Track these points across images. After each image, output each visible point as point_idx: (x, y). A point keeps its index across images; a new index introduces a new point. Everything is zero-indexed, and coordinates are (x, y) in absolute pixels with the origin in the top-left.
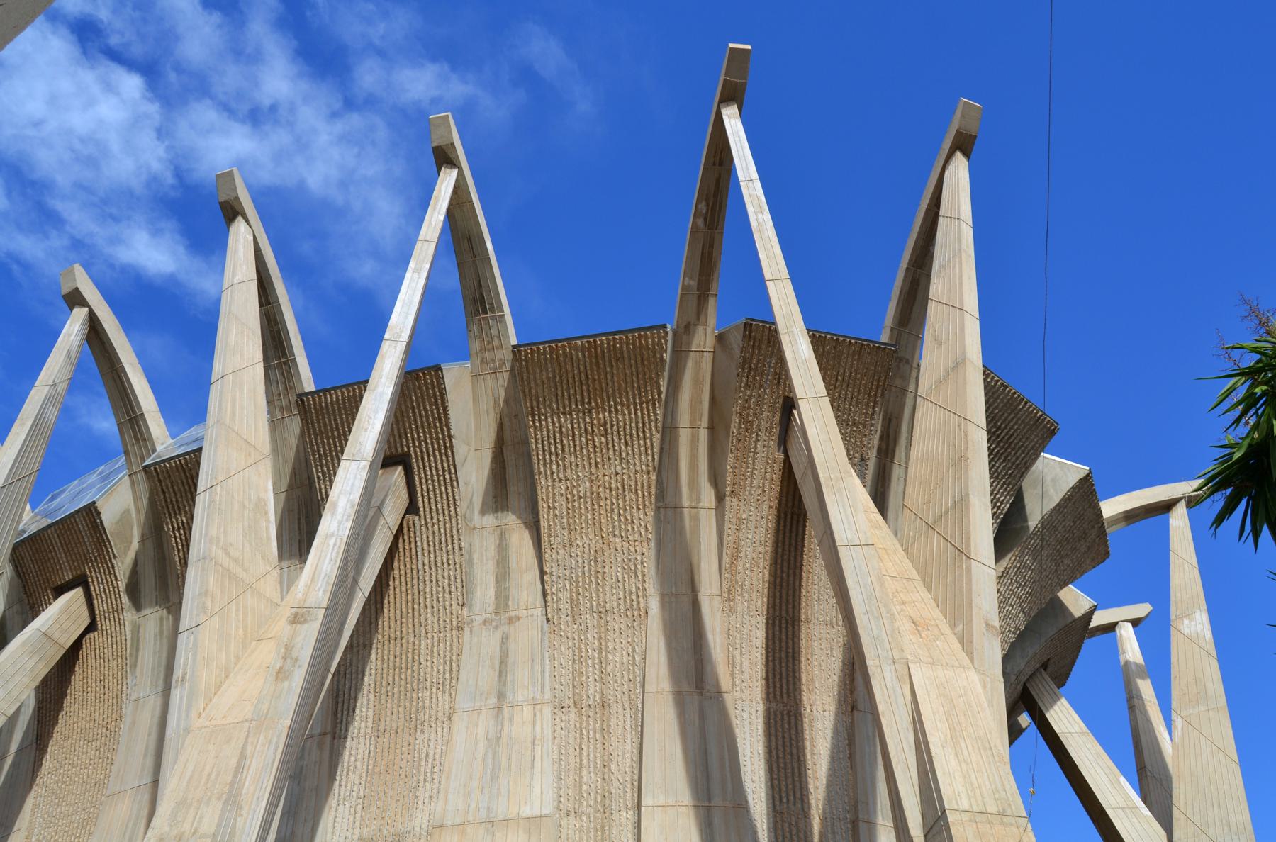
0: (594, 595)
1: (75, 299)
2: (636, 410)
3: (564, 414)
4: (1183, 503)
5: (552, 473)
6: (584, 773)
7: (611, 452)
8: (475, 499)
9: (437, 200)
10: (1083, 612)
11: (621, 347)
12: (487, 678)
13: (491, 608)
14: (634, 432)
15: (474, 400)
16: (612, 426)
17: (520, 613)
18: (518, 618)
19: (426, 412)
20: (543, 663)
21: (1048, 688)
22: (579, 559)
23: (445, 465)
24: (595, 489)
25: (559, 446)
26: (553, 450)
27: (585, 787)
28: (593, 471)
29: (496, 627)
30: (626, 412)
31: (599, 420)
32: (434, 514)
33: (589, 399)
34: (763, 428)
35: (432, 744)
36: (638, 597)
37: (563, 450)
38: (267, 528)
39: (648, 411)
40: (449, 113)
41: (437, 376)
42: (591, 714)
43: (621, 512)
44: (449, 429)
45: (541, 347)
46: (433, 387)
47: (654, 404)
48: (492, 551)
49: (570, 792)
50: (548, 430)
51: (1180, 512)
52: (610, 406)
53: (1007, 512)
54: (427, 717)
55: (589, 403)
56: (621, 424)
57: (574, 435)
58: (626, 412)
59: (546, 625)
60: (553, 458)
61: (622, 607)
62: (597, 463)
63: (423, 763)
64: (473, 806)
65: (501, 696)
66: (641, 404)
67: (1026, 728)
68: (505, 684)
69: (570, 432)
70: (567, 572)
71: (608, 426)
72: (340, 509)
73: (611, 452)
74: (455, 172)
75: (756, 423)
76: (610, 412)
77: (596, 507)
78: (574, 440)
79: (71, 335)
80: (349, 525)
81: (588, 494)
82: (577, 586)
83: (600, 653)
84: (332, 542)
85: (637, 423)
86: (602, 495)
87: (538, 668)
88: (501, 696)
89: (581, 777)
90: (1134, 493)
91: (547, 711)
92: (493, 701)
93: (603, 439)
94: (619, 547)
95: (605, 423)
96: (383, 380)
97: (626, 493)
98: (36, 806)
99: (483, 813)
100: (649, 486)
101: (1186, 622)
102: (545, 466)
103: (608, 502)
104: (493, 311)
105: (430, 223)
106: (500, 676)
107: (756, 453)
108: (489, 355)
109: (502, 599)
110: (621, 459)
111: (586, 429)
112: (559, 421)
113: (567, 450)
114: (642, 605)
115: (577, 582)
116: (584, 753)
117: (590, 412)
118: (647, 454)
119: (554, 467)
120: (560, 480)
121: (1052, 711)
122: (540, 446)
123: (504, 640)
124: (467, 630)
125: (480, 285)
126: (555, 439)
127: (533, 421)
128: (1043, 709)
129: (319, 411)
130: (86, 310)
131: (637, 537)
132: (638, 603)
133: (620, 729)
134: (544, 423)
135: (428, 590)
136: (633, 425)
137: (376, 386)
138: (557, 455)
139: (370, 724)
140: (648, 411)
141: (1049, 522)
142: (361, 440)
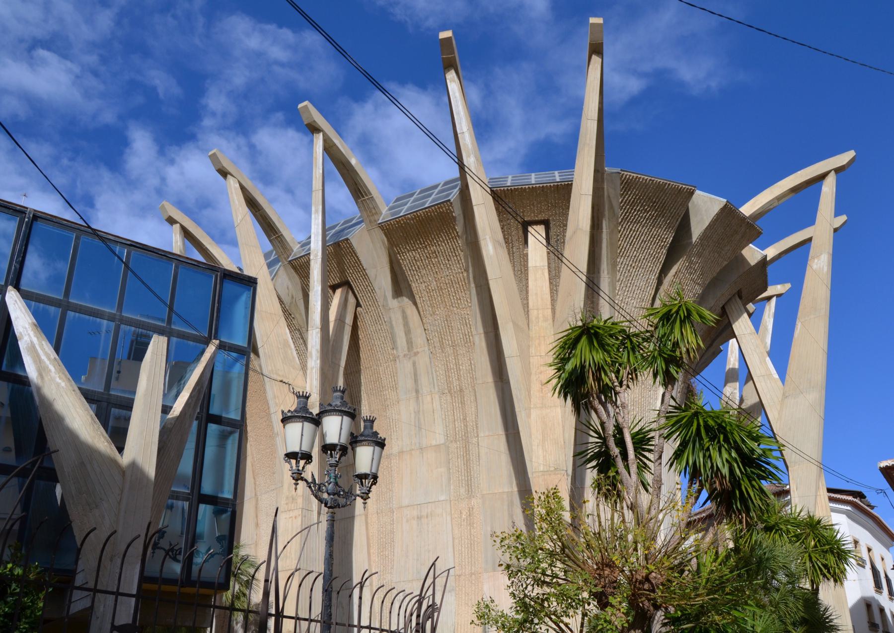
0: (449, 338)
2: (448, 243)
3: (414, 250)
5: (417, 280)
6: (456, 423)
7: (442, 265)
8: (387, 294)
9: (316, 158)
10: (756, 262)
11: (431, 215)
12: (410, 383)
13: (406, 349)
14: (450, 254)
15: (372, 242)
16: (439, 252)
17: (418, 350)
18: (418, 352)
19: (349, 260)
20: (432, 374)
22: (439, 321)
23: (367, 283)
24: (439, 285)
25: (416, 267)
26: (414, 269)
27: (457, 429)
28: (436, 276)
29: (410, 358)
30: (443, 244)
31: (431, 251)
32: (369, 307)
33: (424, 241)
34: (514, 239)
35: (393, 415)
36: (469, 336)
37: (419, 268)
38: (292, 353)
39: (454, 242)
40: (306, 103)
41: (348, 243)
42: (456, 396)
43: (454, 295)
44: (363, 267)
45: (392, 222)
46: (348, 248)
47: (456, 239)
48: (401, 320)
49: (451, 432)
50: (409, 260)
52: (435, 243)
53: (671, 243)
54: (389, 404)
55: (424, 243)
56: (443, 251)
57: (422, 260)
58: (443, 244)
59: (431, 355)
60: (415, 272)
61: (462, 342)
62: (436, 272)
63: (392, 424)
64: (413, 442)
65: (417, 391)
66: (450, 239)
67: (753, 313)
68: (418, 386)
69: (420, 259)
70: (435, 328)
71: (437, 253)
73: (442, 265)
74: (321, 134)
75: (510, 238)
76: (436, 246)
77: (441, 293)
78: (422, 262)
79: (177, 242)
80: (319, 361)
81: (436, 288)
82: (441, 334)
83: (456, 366)
84: (314, 371)
85: (450, 249)
86: (443, 287)
87: (430, 376)
88: (417, 391)
89: (455, 425)
90: (799, 172)
91: (437, 397)
92: (414, 394)
93: (436, 260)
94: (456, 312)
95: (435, 252)
96: (316, 283)
97: (454, 285)
98: (251, 445)
100: (464, 279)
101: (816, 261)
102: (412, 277)
103: (447, 290)
104: (367, 196)
105: (316, 177)
106: (415, 382)
107: (513, 253)
108: (372, 218)
109: (410, 343)
110: (448, 268)
111: (427, 256)
112: (413, 254)
113: (420, 267)
114: (471, 340)
115: (440, 332)
116: (455, 414)
117: (426, 247)
118: (459, 264)
119: (417, 277)
120: (421, 283)
121: (736, 323)
122: (407, 268)
123: (414, 364)
124: (398, 361)
125: (356, 184)
126: (413, 263)
127: (400, 256)
128: (732, 323)
129: (301, 266)
130: (178, 225)
131: (463, 306)
132: (470, 339)
133: (469, 401)
134: (405, 256)
135: (376, 343)
136: (449, 250)
137: (314, 288)
138: (417, 271)
139: (367, 408)
140: (454, 242)
141: (705, 236)
142: (314, 318)
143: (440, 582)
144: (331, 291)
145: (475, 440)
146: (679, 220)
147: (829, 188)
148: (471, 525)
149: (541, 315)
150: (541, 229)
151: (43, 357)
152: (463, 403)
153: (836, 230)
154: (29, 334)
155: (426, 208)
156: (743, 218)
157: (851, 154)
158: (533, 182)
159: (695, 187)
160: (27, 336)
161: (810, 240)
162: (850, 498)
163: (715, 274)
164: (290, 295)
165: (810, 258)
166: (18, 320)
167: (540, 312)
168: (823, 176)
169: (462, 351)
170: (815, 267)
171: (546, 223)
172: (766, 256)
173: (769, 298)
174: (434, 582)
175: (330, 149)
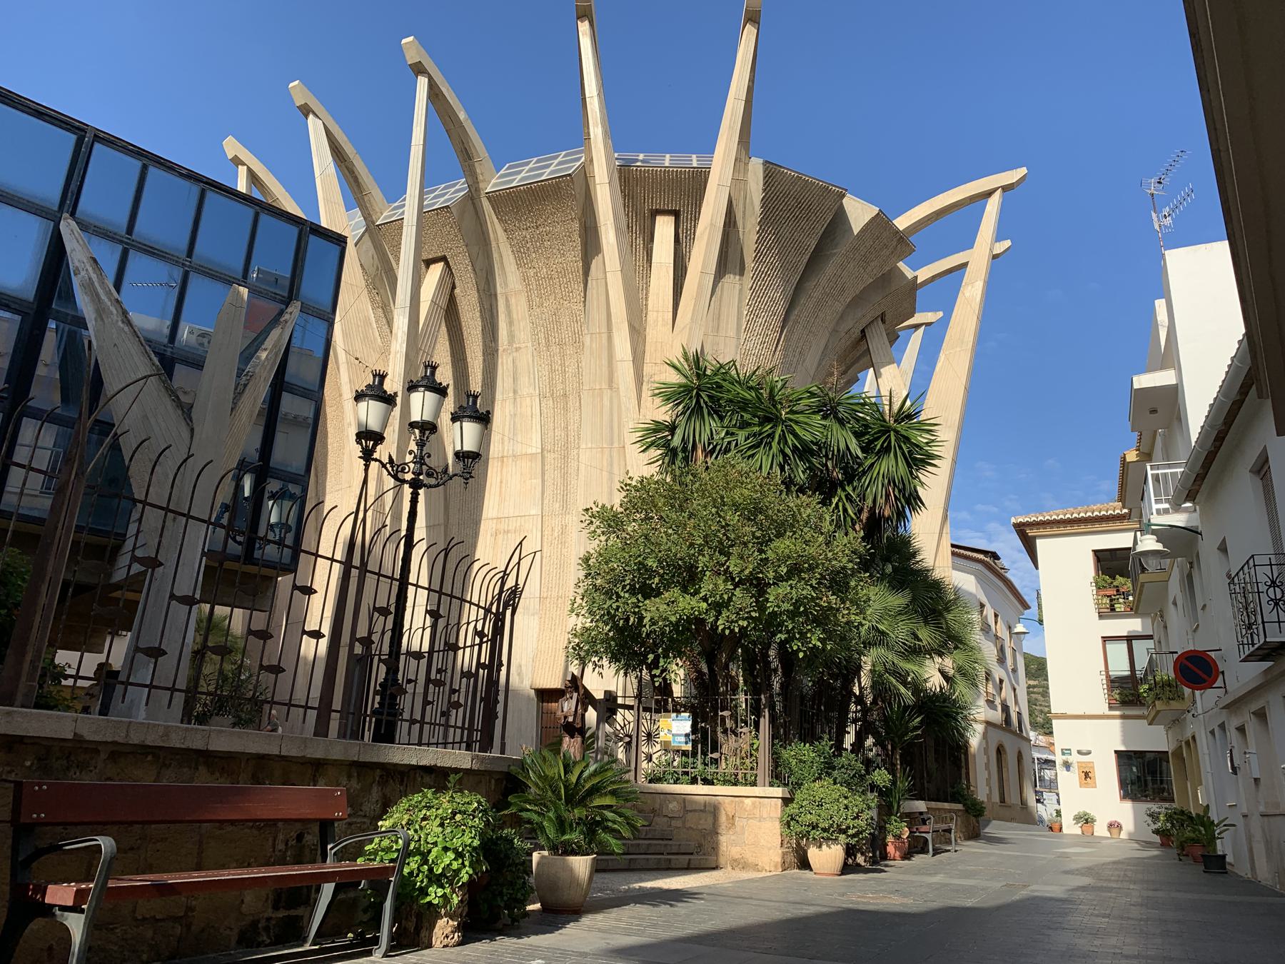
1: (237, 161)
4: (999, 192)
18: (520, 348)
20: (534, 374)
21: (878, 332)
51: (996, 198)
65: (515, 392)
72: (400, 335)
84: (398, 356)
87: (532, 376)
88: (515, 392)
99: (511, 452)
101: (970, 288)
130: (245, 167)
143: (525, 564)
144: (423, 266)
145: (576, 451)
146: (825, 226)
147: (993, 205)
148: (563, 543)
149: (660, 319)
150: (671, 219)
151: (103, 297)
152: (566, 409)
153: (995, 257)
154: (87, 270)
155: (542, 181)
156: (897, 231)
157: (1023, 171)
158: (667, 165)
159: (846, 190)
160: (85, 272)
161: (965, 265)
162: (981, 556)
163: (857, 292)
164: (375, 266)
165: (963, 284)
166: (74, 252)
167: (660, 314)
168: (989, 194)
169: (570, 350)
170: (967, 294)
171: (676, 214)
172: (916, 277)
173: (917, 327)
174: (519, 563)
175: (434, 94)
